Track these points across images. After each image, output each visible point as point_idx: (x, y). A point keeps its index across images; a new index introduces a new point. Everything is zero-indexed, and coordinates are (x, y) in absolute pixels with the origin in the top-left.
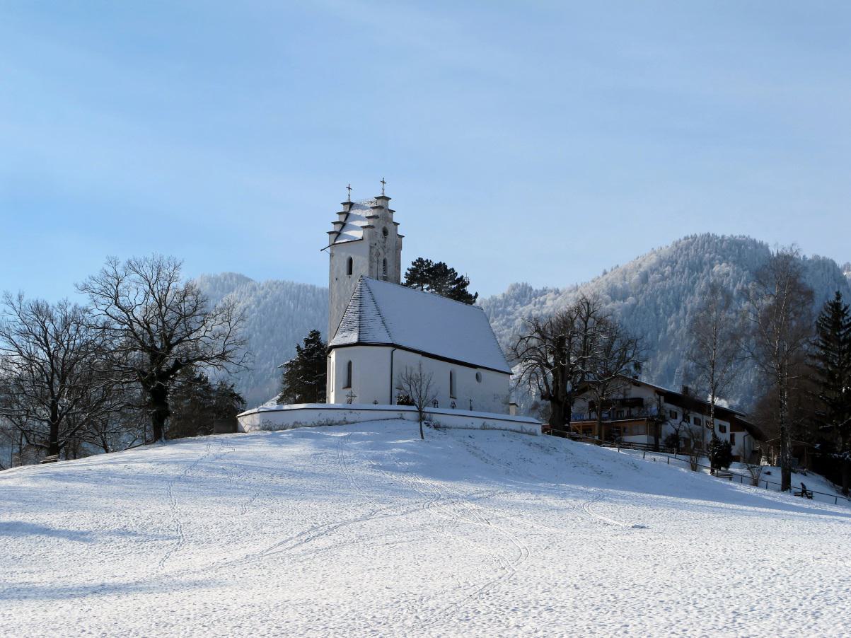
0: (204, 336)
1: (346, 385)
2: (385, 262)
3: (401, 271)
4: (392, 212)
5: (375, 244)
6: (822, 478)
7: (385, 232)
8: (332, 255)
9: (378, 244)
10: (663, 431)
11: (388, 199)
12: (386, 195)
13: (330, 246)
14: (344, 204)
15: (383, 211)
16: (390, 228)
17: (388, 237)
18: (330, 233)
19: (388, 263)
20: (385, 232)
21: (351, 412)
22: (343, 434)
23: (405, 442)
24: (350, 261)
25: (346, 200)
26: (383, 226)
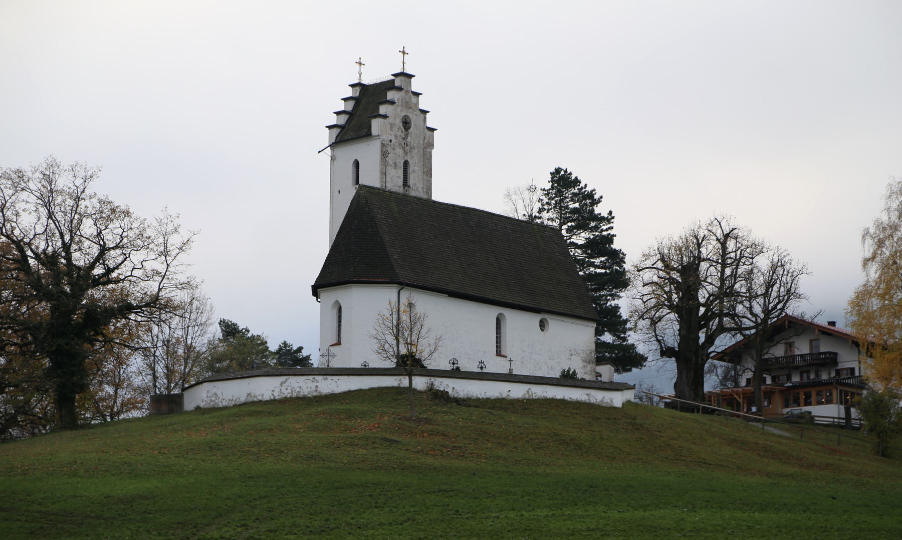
0: (131, 276)
1: (335, 341)
2: (406, 164)
3: (711, 348)
4: (417, 94)
5: (391, 141)
6: (492, 398)
7: (406, 123)
8: (333, 159)
9: (394, 141)
10: (394, 189)
11: (410, 76)
12: (408, 71)
13: (329, 146)
14: (353, 86)
15: (402, 93)
16: (414, 119)
17: (411, 130)
18: (330, 127)
19: (411, 168)
20: (406, 123)
21: (281, 372)
22: (786, 434)
23: (171, 415)
24: (357, 164)
25: (356, 81)
26: (404, 114)
